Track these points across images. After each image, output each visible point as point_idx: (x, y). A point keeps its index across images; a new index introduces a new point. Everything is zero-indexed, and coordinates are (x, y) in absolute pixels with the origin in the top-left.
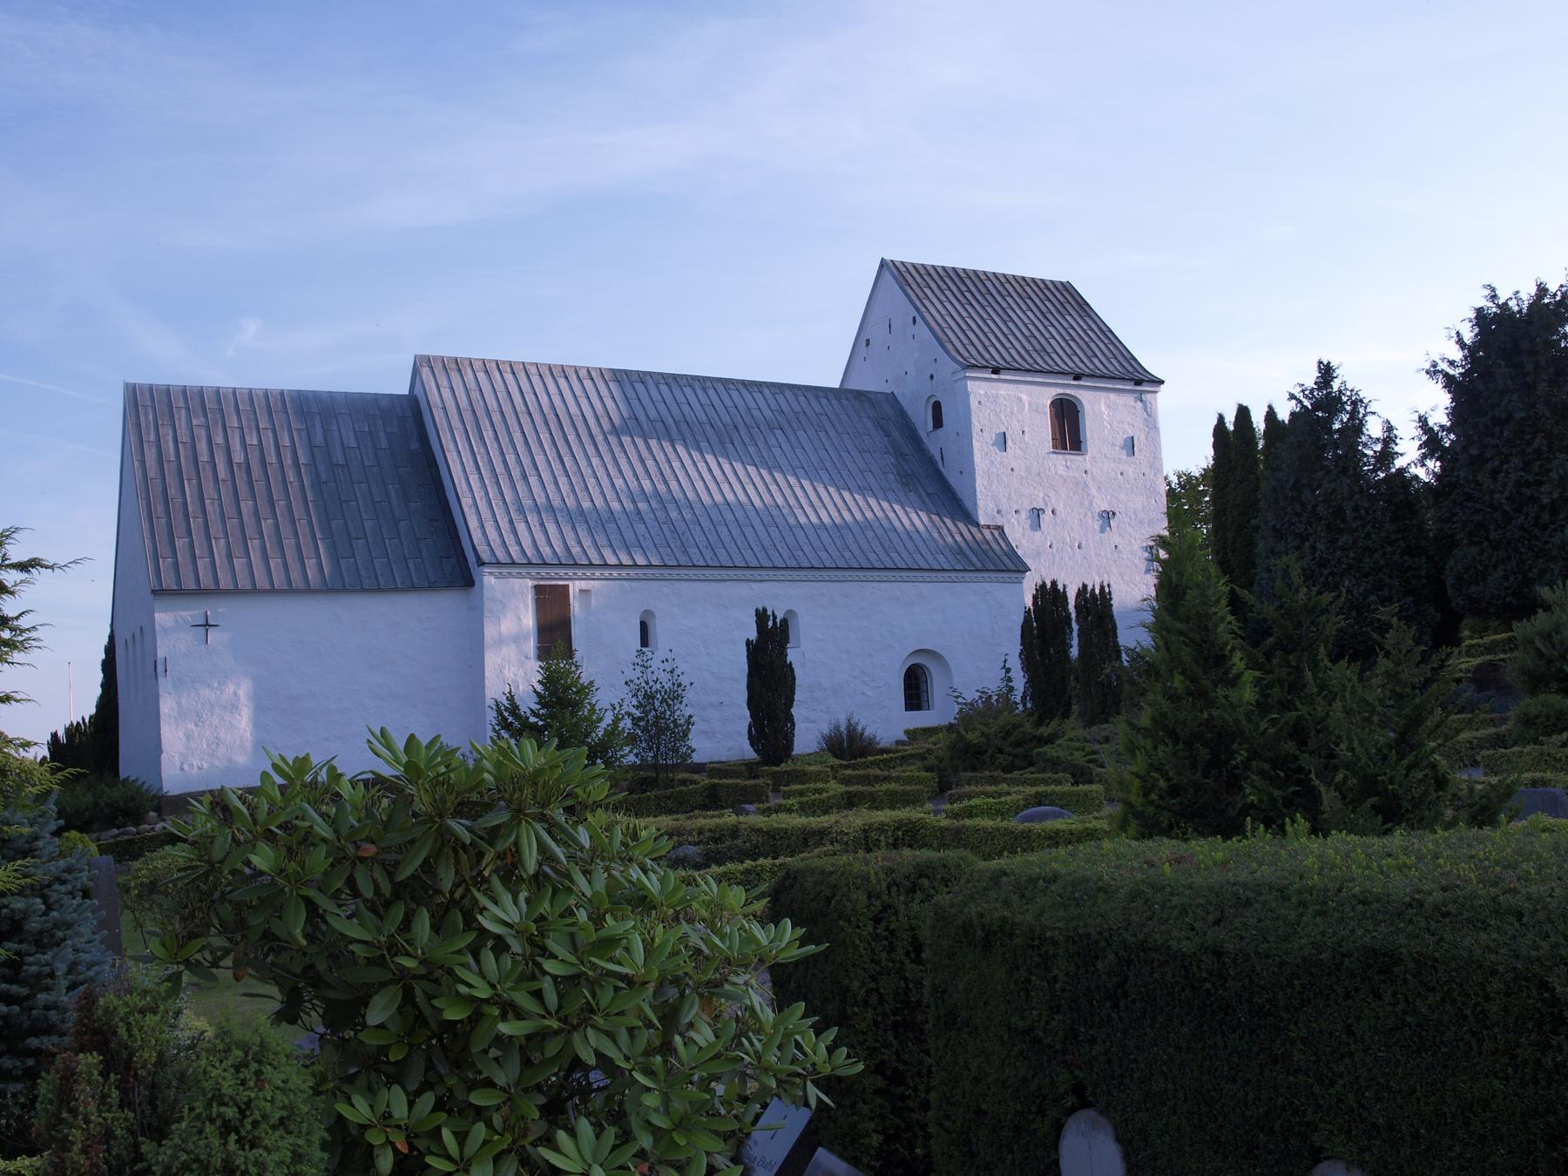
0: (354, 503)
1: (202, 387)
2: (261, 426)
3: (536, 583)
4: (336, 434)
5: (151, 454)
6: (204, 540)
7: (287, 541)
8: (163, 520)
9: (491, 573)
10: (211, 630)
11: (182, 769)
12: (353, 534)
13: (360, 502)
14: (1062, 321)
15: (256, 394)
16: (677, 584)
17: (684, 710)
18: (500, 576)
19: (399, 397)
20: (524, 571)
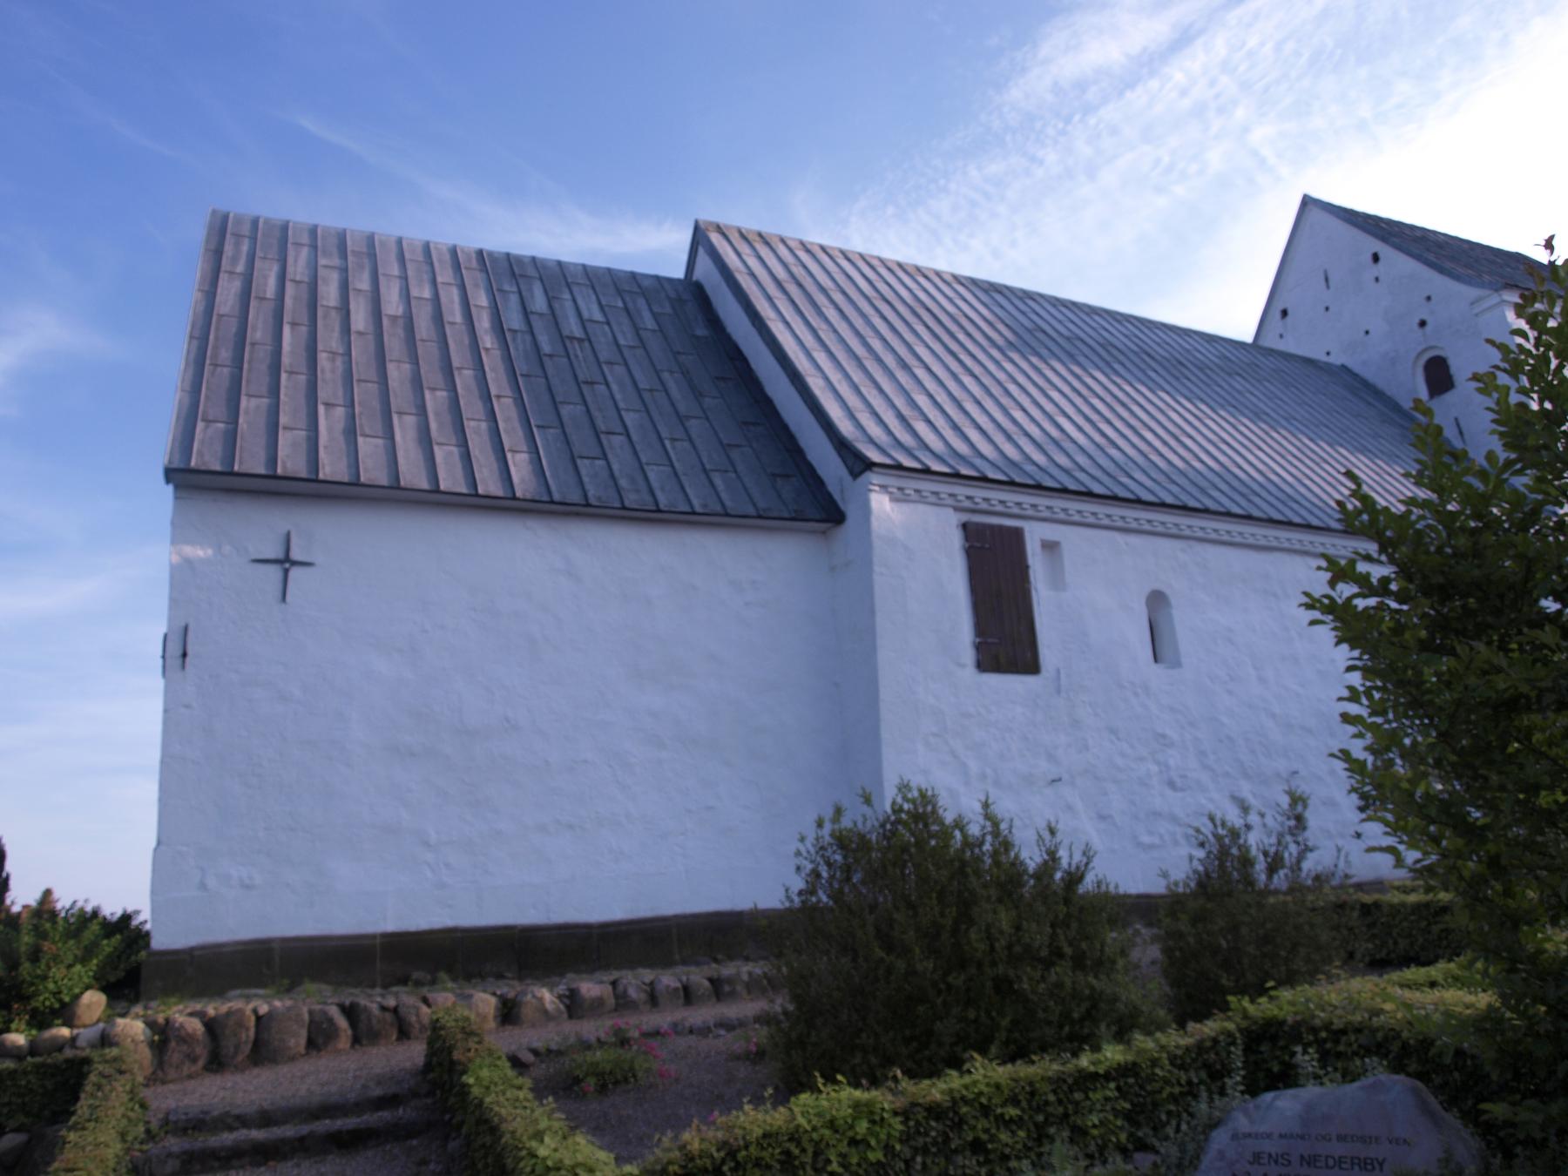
0: (603, 387)
1: (345, 230)
2: (439, 279)
3: (965, 517)
4: (569, 304)
5: (228, 291)
6: (303, 401)
7: (473, 424)
8: (226, 371)
9: (884, 487)
10: (295, 573)
11: (203, 886)
12: (601, 426)
13: (614, 387)
14: (1320, 471)
15: (436, 248)
16: (1198, 547)
17: (1067, 859)
18: (900, 497)
19: (670, 280)
20: (944, 488)
